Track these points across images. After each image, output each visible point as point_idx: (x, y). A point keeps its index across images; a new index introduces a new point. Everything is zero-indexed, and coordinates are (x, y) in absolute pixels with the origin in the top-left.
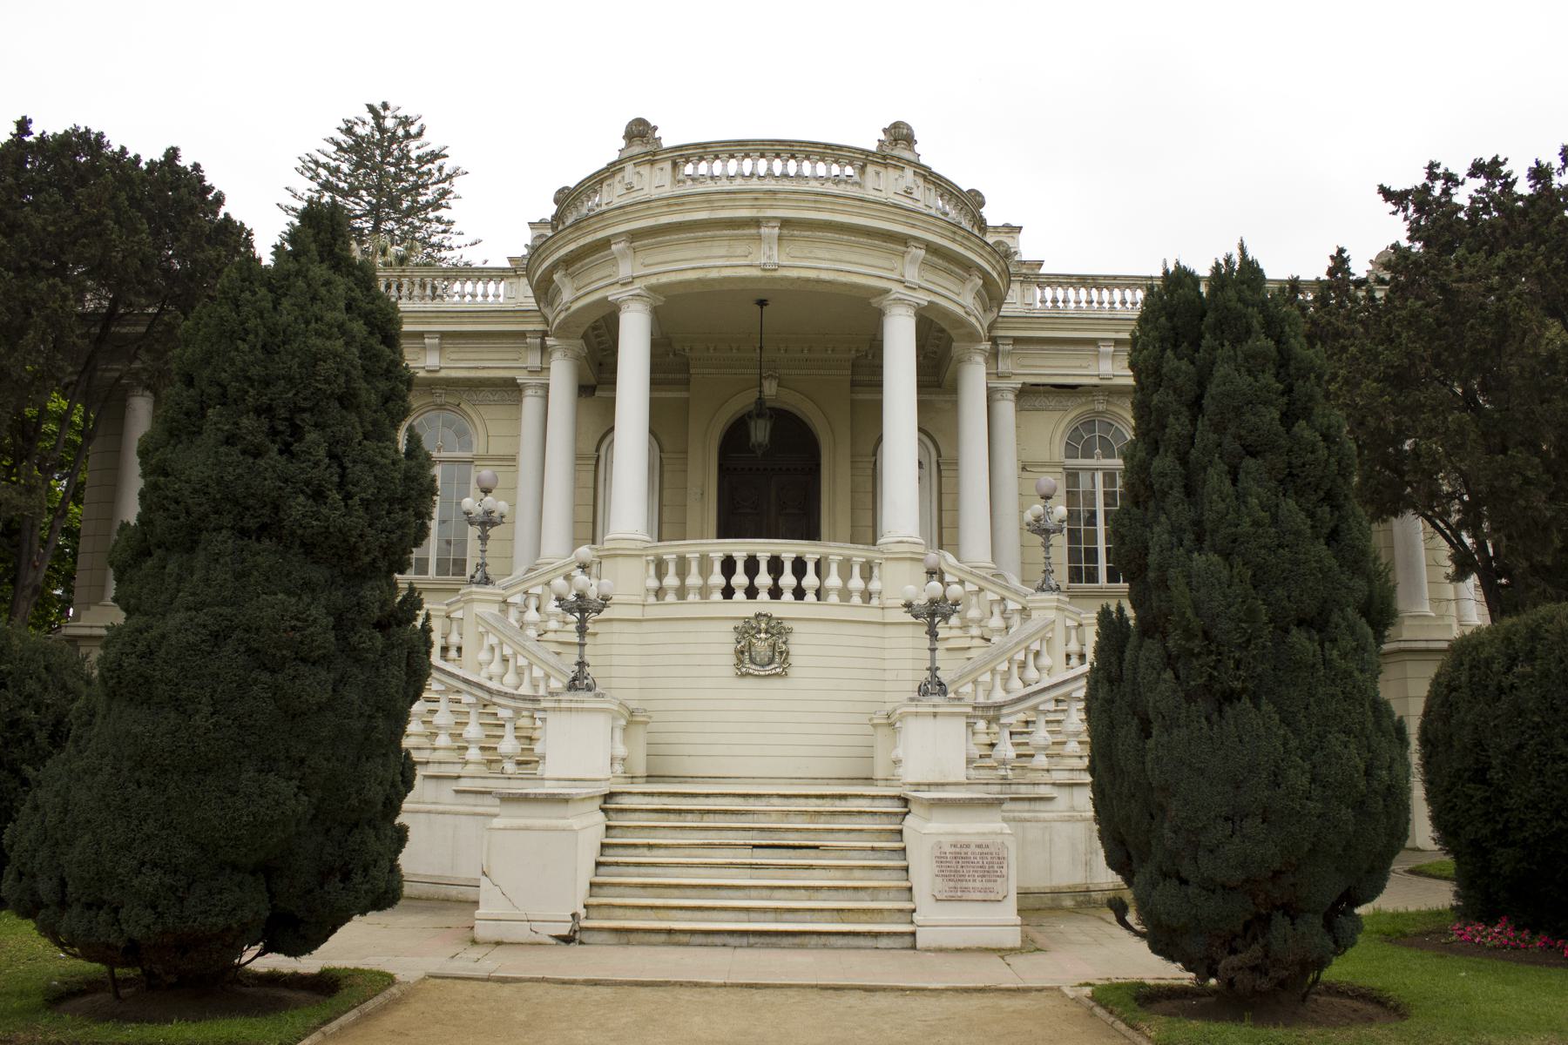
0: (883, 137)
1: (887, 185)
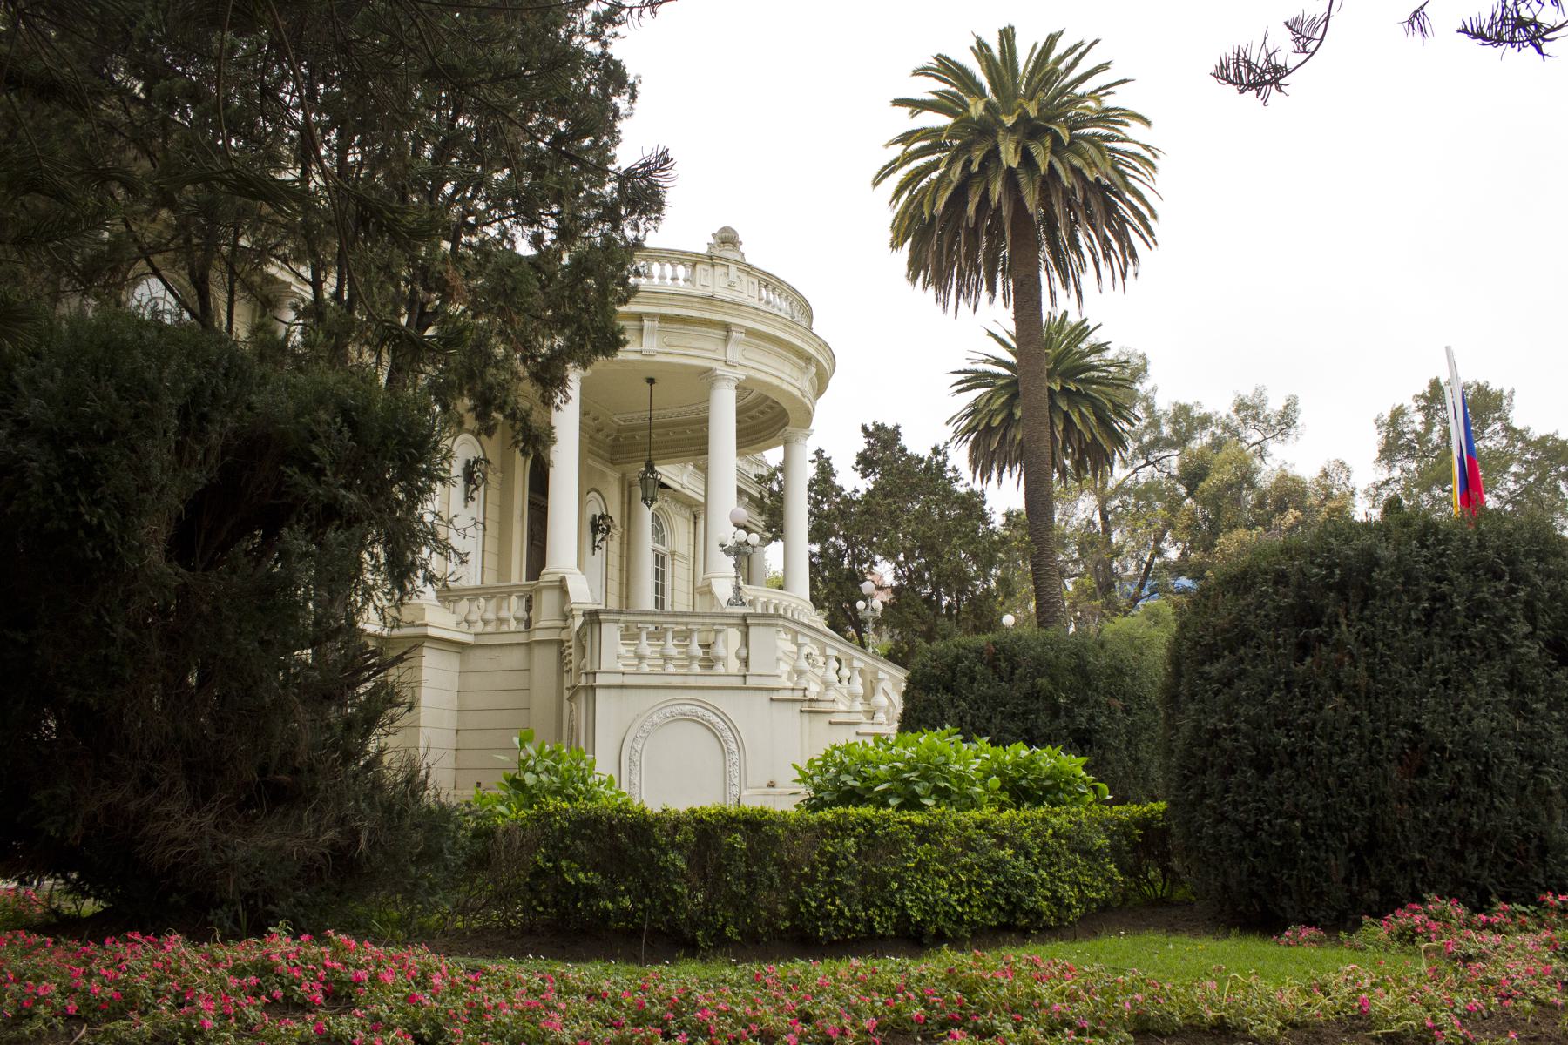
0: (712, 241)
1: (713, 282)
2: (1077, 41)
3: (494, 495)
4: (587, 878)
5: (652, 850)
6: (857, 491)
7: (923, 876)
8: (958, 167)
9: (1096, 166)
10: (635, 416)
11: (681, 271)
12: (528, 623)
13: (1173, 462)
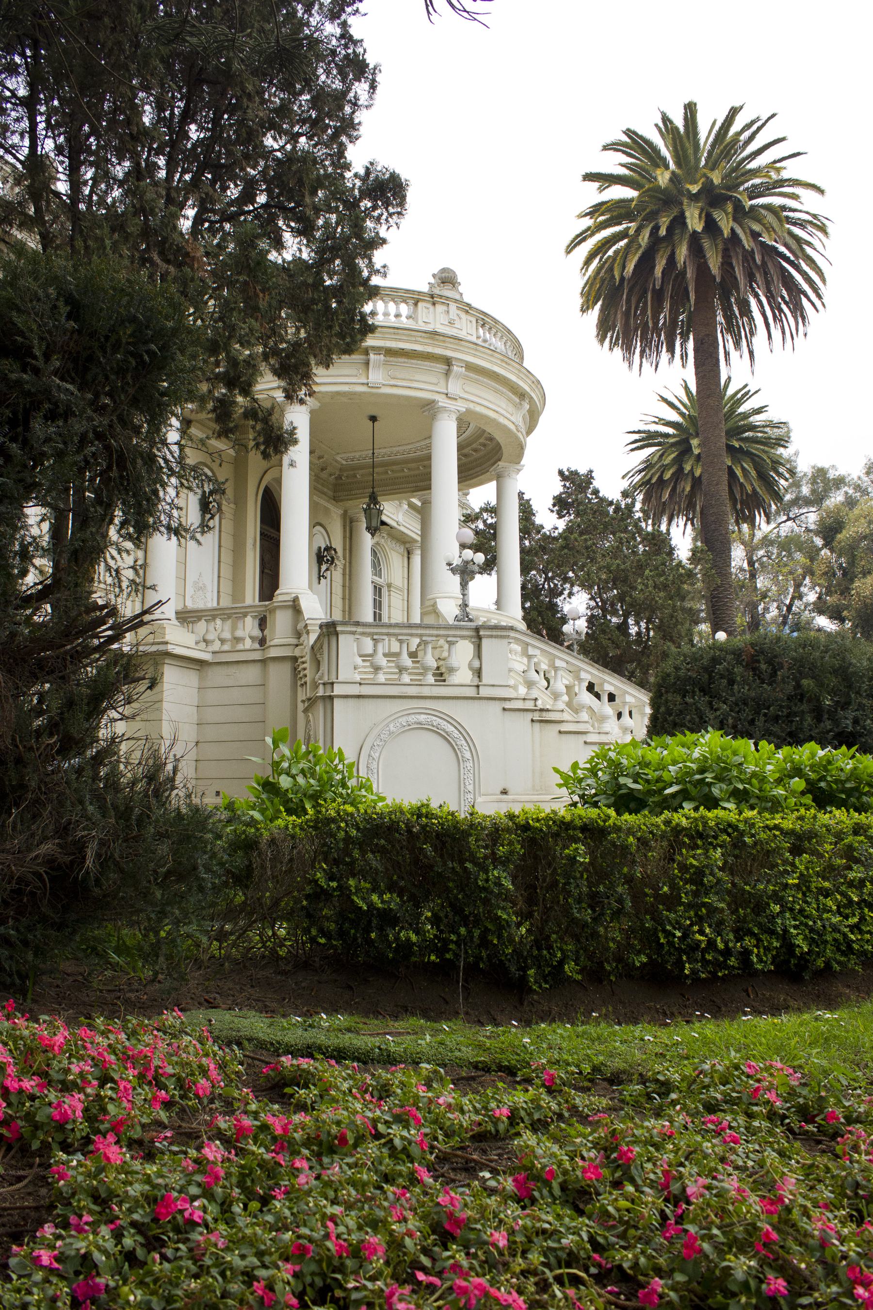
0: (432, 281)
2: (753, 117)
3: (228, 525)
4: (383, 902)
5: (468, 865)
6: (556, 528)
7: (804, 894)
8: (646, 234)
9: (774, 231)
10: (357, 455)
11: (404, 309)
12: (262, 642)
13: (812, 517)
